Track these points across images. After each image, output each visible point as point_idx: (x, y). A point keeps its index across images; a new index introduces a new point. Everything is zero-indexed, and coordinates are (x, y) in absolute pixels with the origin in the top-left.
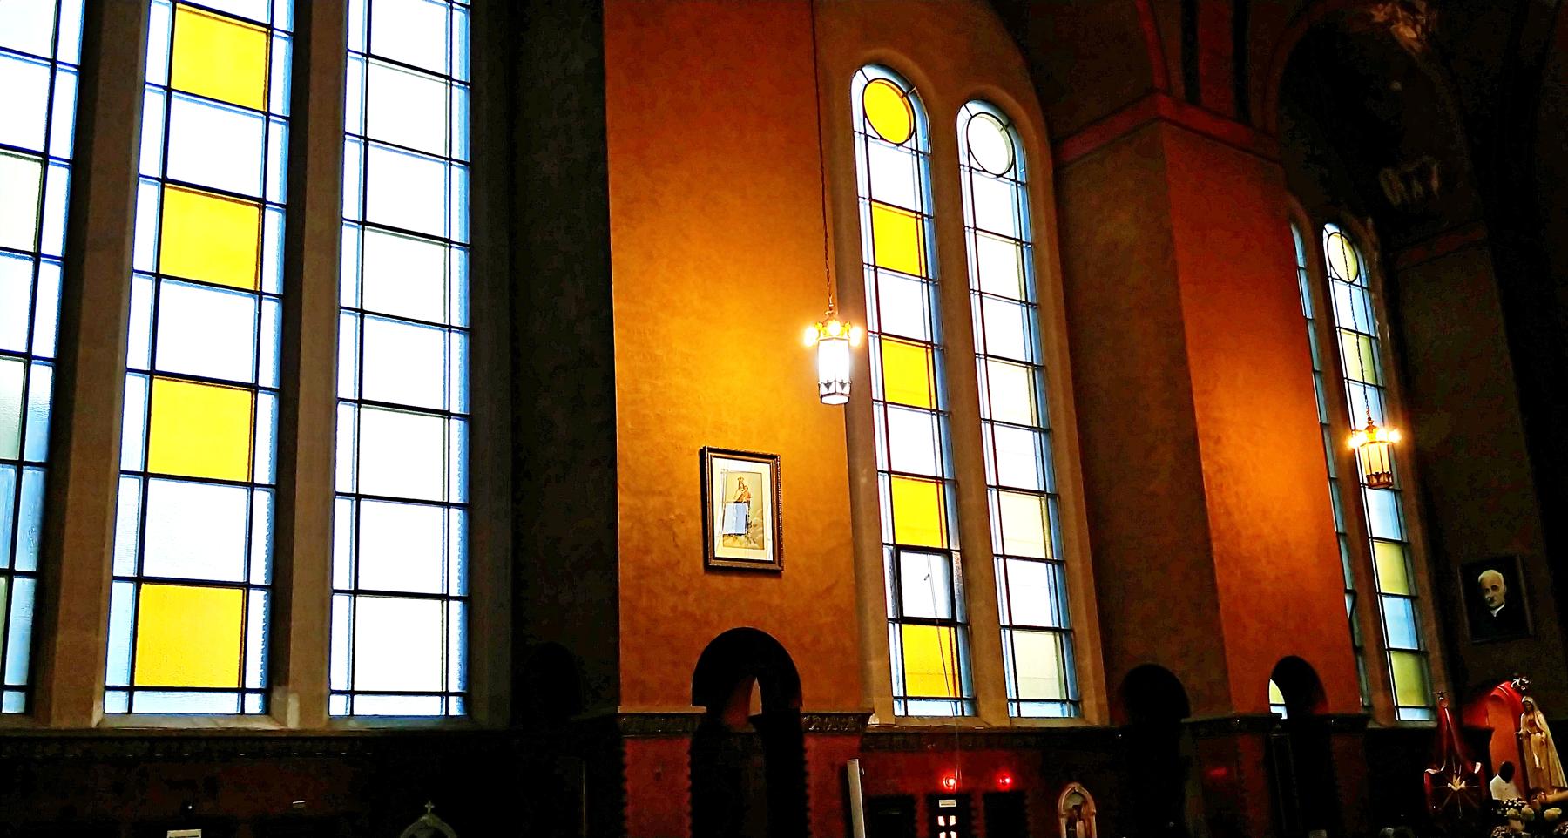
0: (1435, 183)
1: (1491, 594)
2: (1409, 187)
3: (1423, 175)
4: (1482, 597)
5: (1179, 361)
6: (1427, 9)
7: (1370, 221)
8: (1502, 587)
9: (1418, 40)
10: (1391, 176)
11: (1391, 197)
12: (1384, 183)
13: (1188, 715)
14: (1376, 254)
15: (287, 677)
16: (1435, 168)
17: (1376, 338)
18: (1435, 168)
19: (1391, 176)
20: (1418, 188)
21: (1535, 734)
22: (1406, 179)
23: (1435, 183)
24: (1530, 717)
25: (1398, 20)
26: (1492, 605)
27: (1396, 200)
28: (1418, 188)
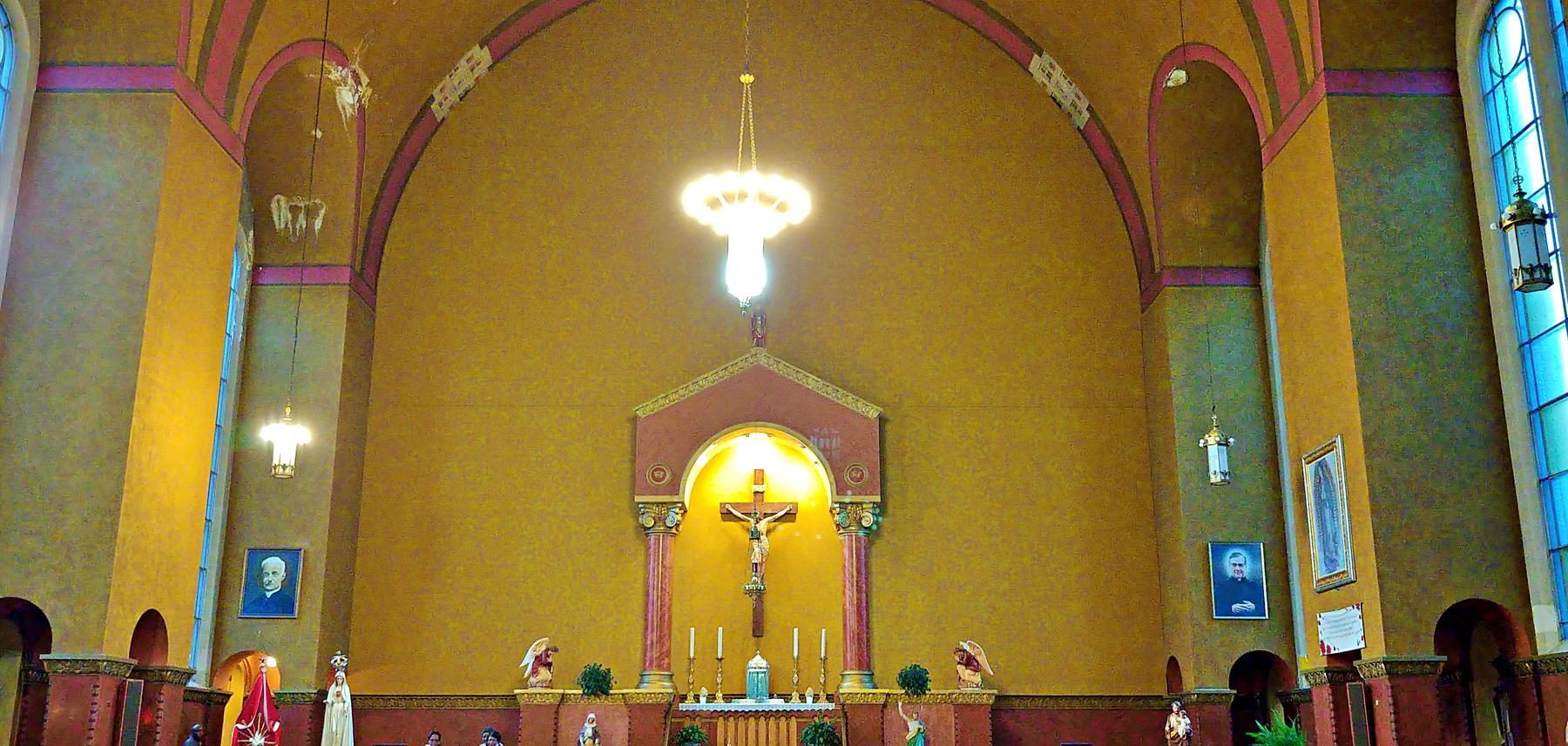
0: (318, 224)
1: (271, 577)
2: (295, 219)
3: (311, 213)
4: (262, 578)
5: (135, 321)
6: (369, 84)
7: (251, 233)
8: (283, 573)
9: (353, 106)
10: (283, 204)
11: (276, 219)
12: (274, 205)
13: (48, 651)
14: (249, 264)
15: (900, 675)
16: (322, 212)
17: (229, 336)
18: (322, 212)
19: (283, 204)
20: (302, 221)
21: (339, 703)
22: (294, 210)
23: (318, 224)
24: (339, 689)
25: (346, 84)
26: (268, 588)
27: (279, 224)
28: (302, 221)
